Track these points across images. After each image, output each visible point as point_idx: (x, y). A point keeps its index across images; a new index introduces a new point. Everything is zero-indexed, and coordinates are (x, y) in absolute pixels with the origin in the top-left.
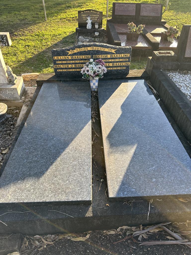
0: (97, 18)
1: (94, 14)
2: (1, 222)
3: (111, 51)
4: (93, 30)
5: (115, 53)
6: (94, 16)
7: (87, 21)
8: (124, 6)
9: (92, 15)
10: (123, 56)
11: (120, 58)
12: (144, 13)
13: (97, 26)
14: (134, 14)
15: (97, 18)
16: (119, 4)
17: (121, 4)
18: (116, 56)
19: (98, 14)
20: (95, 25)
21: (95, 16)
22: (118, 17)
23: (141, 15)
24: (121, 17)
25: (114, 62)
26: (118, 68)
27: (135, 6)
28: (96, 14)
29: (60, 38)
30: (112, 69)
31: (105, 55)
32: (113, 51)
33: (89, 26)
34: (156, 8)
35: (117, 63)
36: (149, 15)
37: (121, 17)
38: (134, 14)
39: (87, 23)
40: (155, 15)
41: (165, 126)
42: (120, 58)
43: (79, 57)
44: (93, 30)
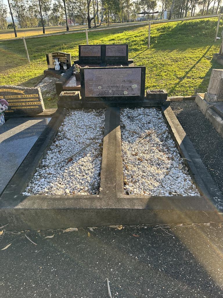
1: (62, 56)
2: (33, 242)
3: (20, 92)
5: (24, 93)
6: (62, 58)
10: (32, 96)
11: (30, 98)
12: (109, 54)
14: (99, 55)
17: (86, 46)
18: (26, 96)
19: (66, 56)
21: (63, 58)
22: (84, 58)
23: (106, 56)
24: (87, 58)
25: (26, 102)
26: (31, 107)
27: (100, 47)
29: (27, 79)
30: (25, 107)
31: (16, 96)
32: (22, 92)
34: (121, 49)
35: (29, 103)
36: (114, 55)
38: (99, 55)
40: (121, 55)
42: (30, 98)
43: (28, 96)
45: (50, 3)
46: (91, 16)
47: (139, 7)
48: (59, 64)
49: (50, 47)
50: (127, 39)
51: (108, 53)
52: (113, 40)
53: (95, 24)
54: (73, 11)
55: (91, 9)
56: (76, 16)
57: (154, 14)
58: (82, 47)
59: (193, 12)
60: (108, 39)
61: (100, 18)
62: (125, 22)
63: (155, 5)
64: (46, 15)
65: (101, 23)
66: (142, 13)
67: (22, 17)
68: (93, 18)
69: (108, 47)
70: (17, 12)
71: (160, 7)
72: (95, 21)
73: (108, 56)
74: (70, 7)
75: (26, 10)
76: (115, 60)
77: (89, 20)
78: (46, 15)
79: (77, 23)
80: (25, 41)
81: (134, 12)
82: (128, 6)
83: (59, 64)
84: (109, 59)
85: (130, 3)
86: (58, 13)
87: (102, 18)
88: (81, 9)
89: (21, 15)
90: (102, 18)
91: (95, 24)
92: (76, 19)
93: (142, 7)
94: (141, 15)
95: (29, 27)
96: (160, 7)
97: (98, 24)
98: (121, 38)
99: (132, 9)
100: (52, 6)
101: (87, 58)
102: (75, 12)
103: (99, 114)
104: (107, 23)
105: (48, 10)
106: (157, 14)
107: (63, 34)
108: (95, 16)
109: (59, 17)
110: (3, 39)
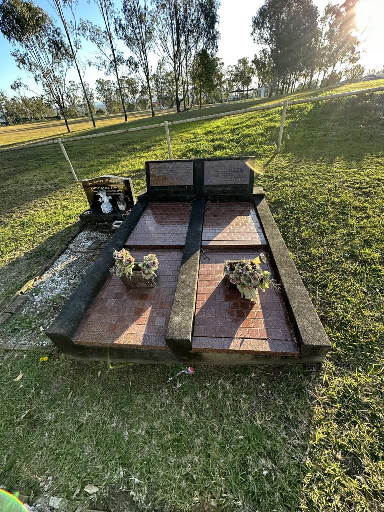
12: (211, 179)
14: (190, 182)
22: (158, 190)
23: (206, 184)
24: (164, 190)
27: (191, 165)
36: (224, 183)
38: (190, 182)
45: (137, 85)
46: (181, 98)
47: (233, 85)
48: (110, 200)
49: (120, 146)
50: (233, 131)
51: (210, 178)
52: (211, 132)
53: (185, 107)
54: (162, 92)
55: (181, 91)
56: (166, 99)
57: (249, 92)
58: (153, 167)
59: (293, 88)
60: (204, 132)
61: (191, 100)
62: (217, 103)
63: (251, 81)
64: (135, 98)
65: (192, 105)
66: (236, 92)
67: (110, 102)
68: (182, 100)
69: (208, 165)
70: (105, 96)
71: (255, 83)
72: (185, 102)
73: (210, 184)
74: (159, 88)
75: (113, 94)
76: (224, 193)
77: (178, 102)
78: (135, 98)
79: (167, 106)
80: (62, 146)
81: (228, 91)
82: (221, 84)
83: (110, 200)
84: (211, 191)
85: (223, 80)
86: (147, 96)
87: (193, 99)
88: (170, 90)
89: (109, 100)
90: (193, 99)
91: (185, 107)
92: (166, 102)
93: (236, 84)
94: (234, 94)
95: (117, 113)
96: (255, 83)
97: (189, 106)
98: (223, 129)
99: (225, 87)
100: (140, 88)
101: (164, 190)
102: (165, 94)
103: (182, 223)
104: (198, 105)
105: (136, 93)
106: (252, 92)
107: (125, 132)
108: (185, 96)
109: (148, 100)
110: (22, 143)
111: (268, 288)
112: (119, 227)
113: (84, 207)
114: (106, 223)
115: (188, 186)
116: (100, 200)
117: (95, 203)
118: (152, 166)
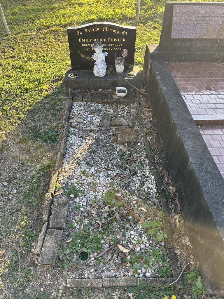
0: (120, 45)
1: (112, 35)
4: (111, 79)
7: (94, 57)
8: (200, 13)
9: (107, 40)
13: (120, 68)
15: (120, 45)
16: (184, 6)
17: (191, 8)
20: (116, 66)
22: (179, 44)
28: (120, 36)
33: (101, 70)
37: (187, 44)
39: (95, 61)
41: (28, 132)
44: (111, 79)
58: (178, 10)
111: (107, 56)
112: (123, 95)
113: (61, 63)
114: (100, 90)
115: (220, 39)
116: (92, 55)
117: (81, 63)
118: (177, 10)
